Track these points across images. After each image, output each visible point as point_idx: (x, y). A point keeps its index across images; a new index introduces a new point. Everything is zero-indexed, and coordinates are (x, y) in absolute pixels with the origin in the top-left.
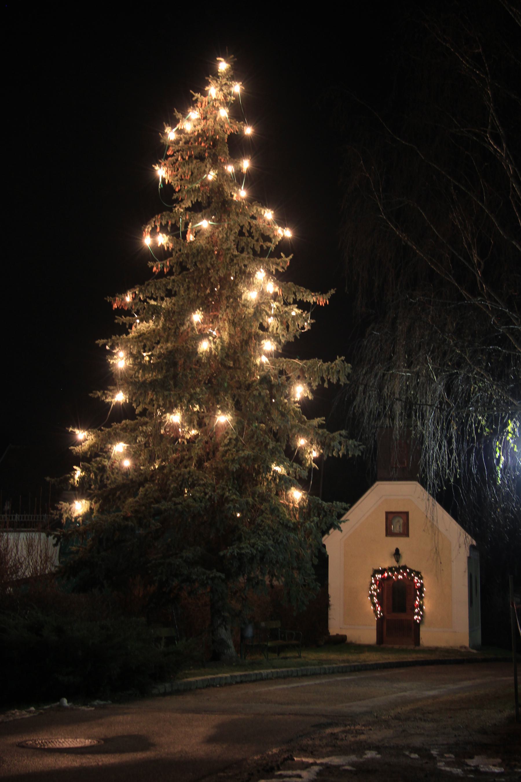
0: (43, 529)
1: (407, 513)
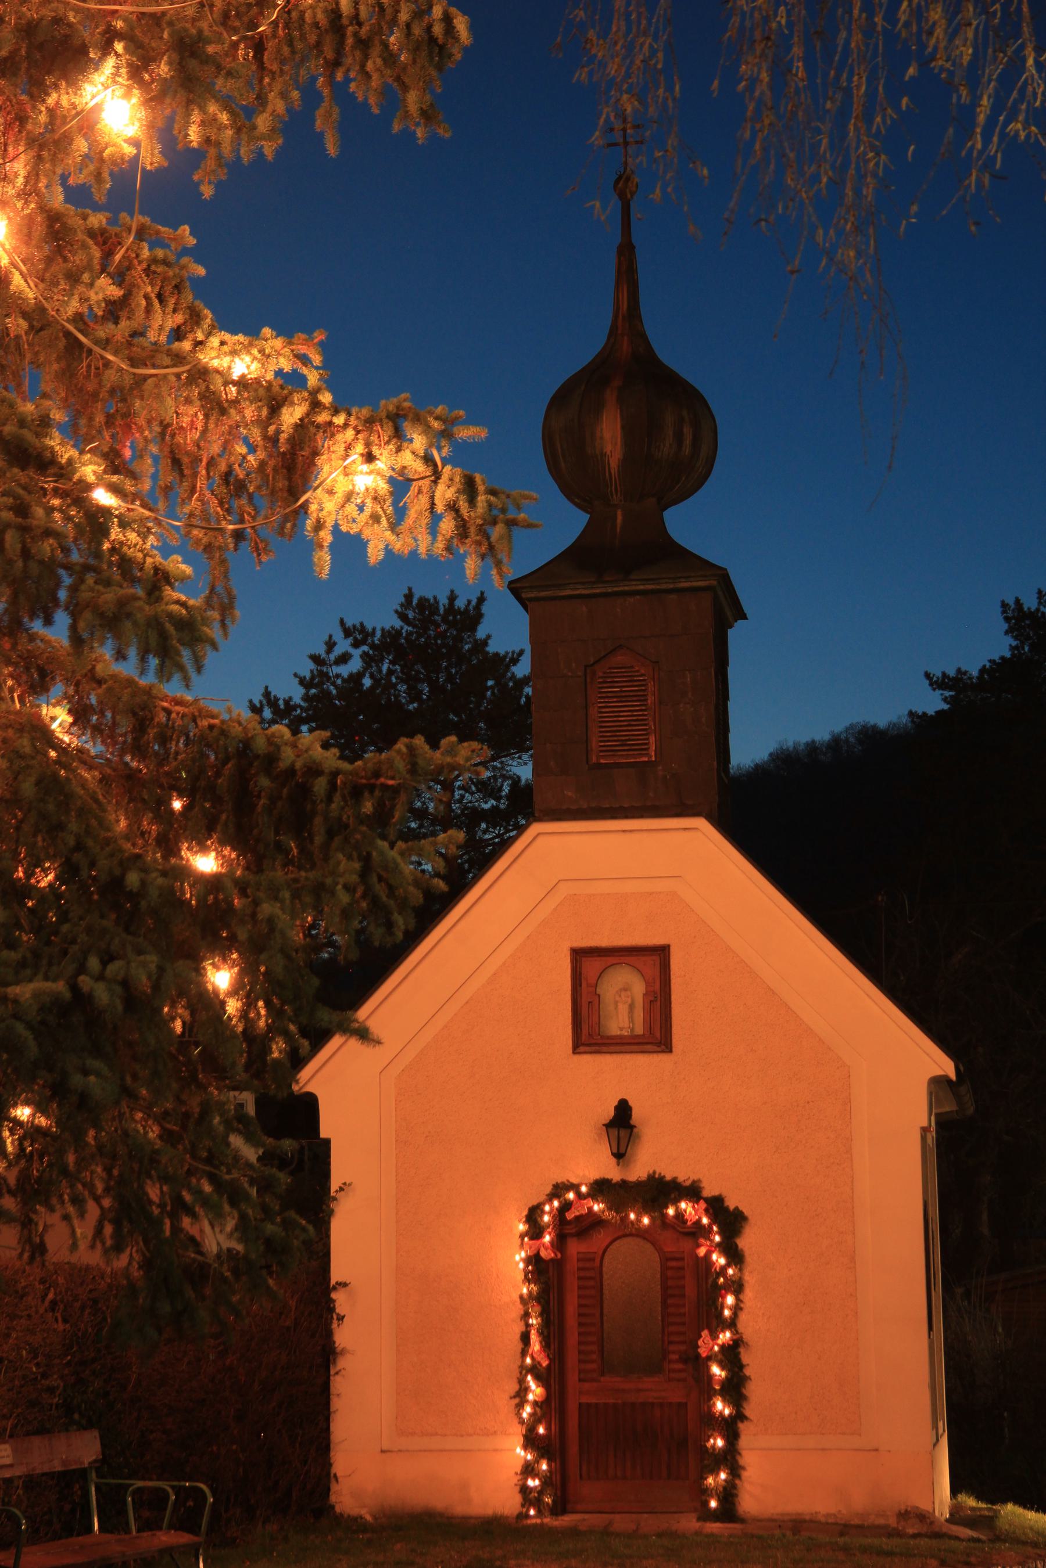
0: (478, 740)
1: (662, 953)
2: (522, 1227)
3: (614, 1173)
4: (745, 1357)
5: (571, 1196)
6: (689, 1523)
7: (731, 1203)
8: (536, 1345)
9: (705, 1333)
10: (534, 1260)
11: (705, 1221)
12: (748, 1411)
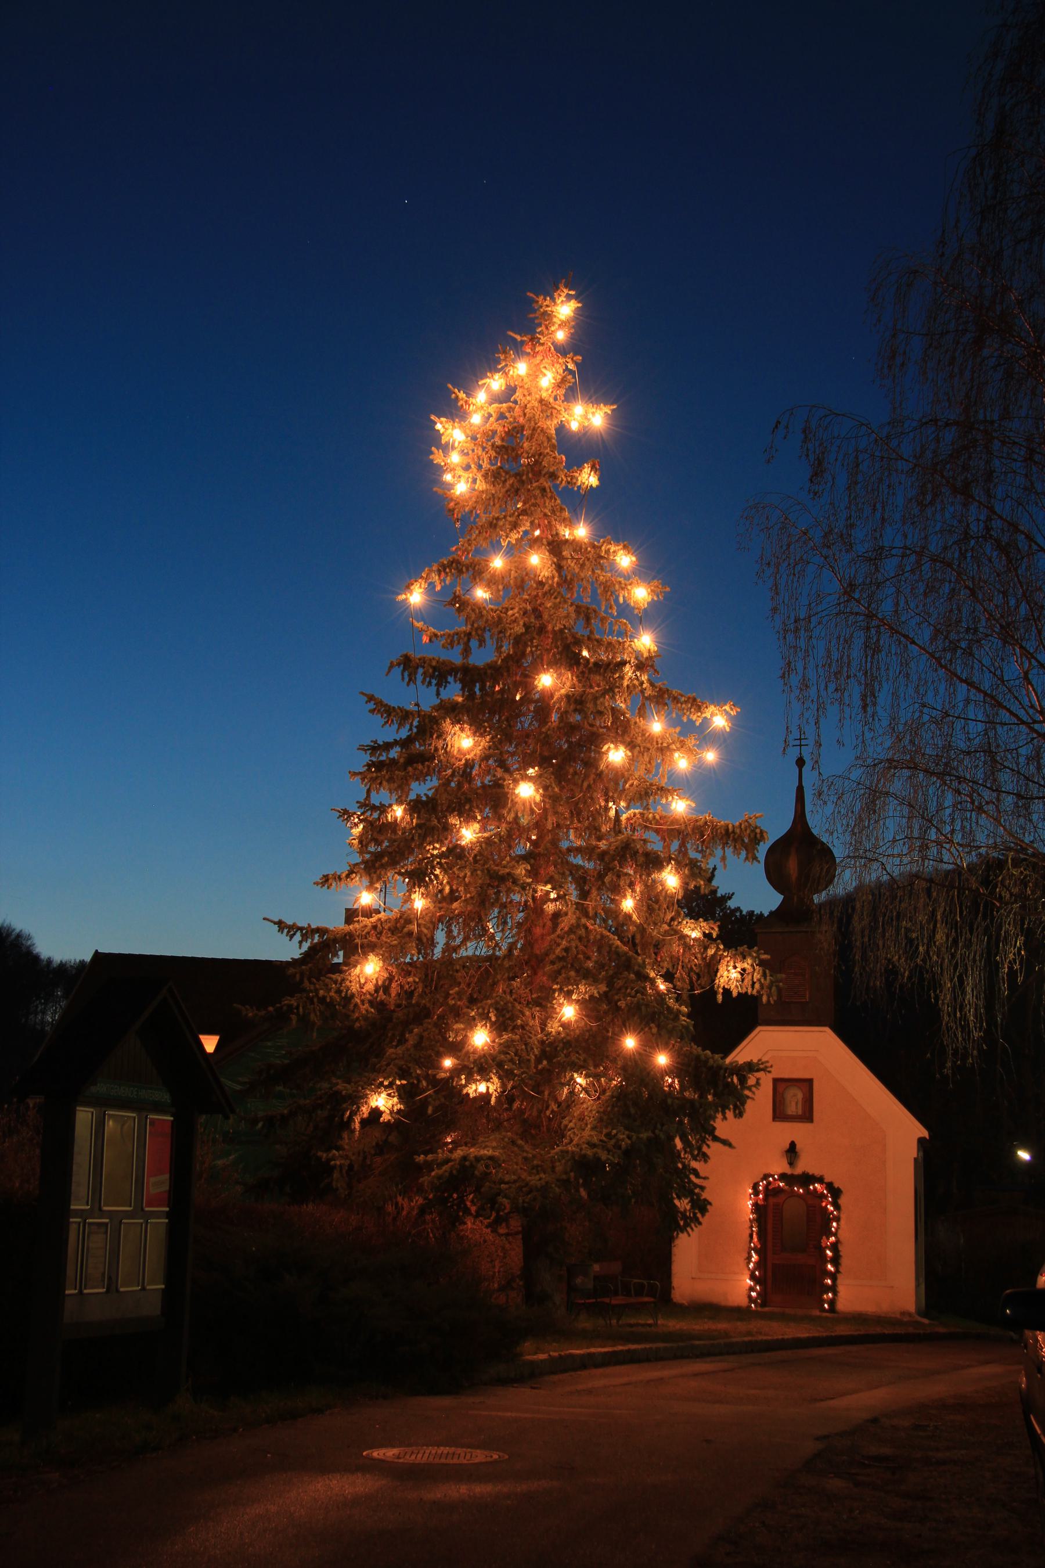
1: (810, 1082)
2: (750, 1191)
3: (788, 1170)
4: (840, 1248)
5: (771, 1179)
6: (816, 1312)
7: (836, 1185)
8: (755, 1239)
9: (824, 1237)
10: (755, 1205)
11: (825, 1192)
12: (841, 1270)
